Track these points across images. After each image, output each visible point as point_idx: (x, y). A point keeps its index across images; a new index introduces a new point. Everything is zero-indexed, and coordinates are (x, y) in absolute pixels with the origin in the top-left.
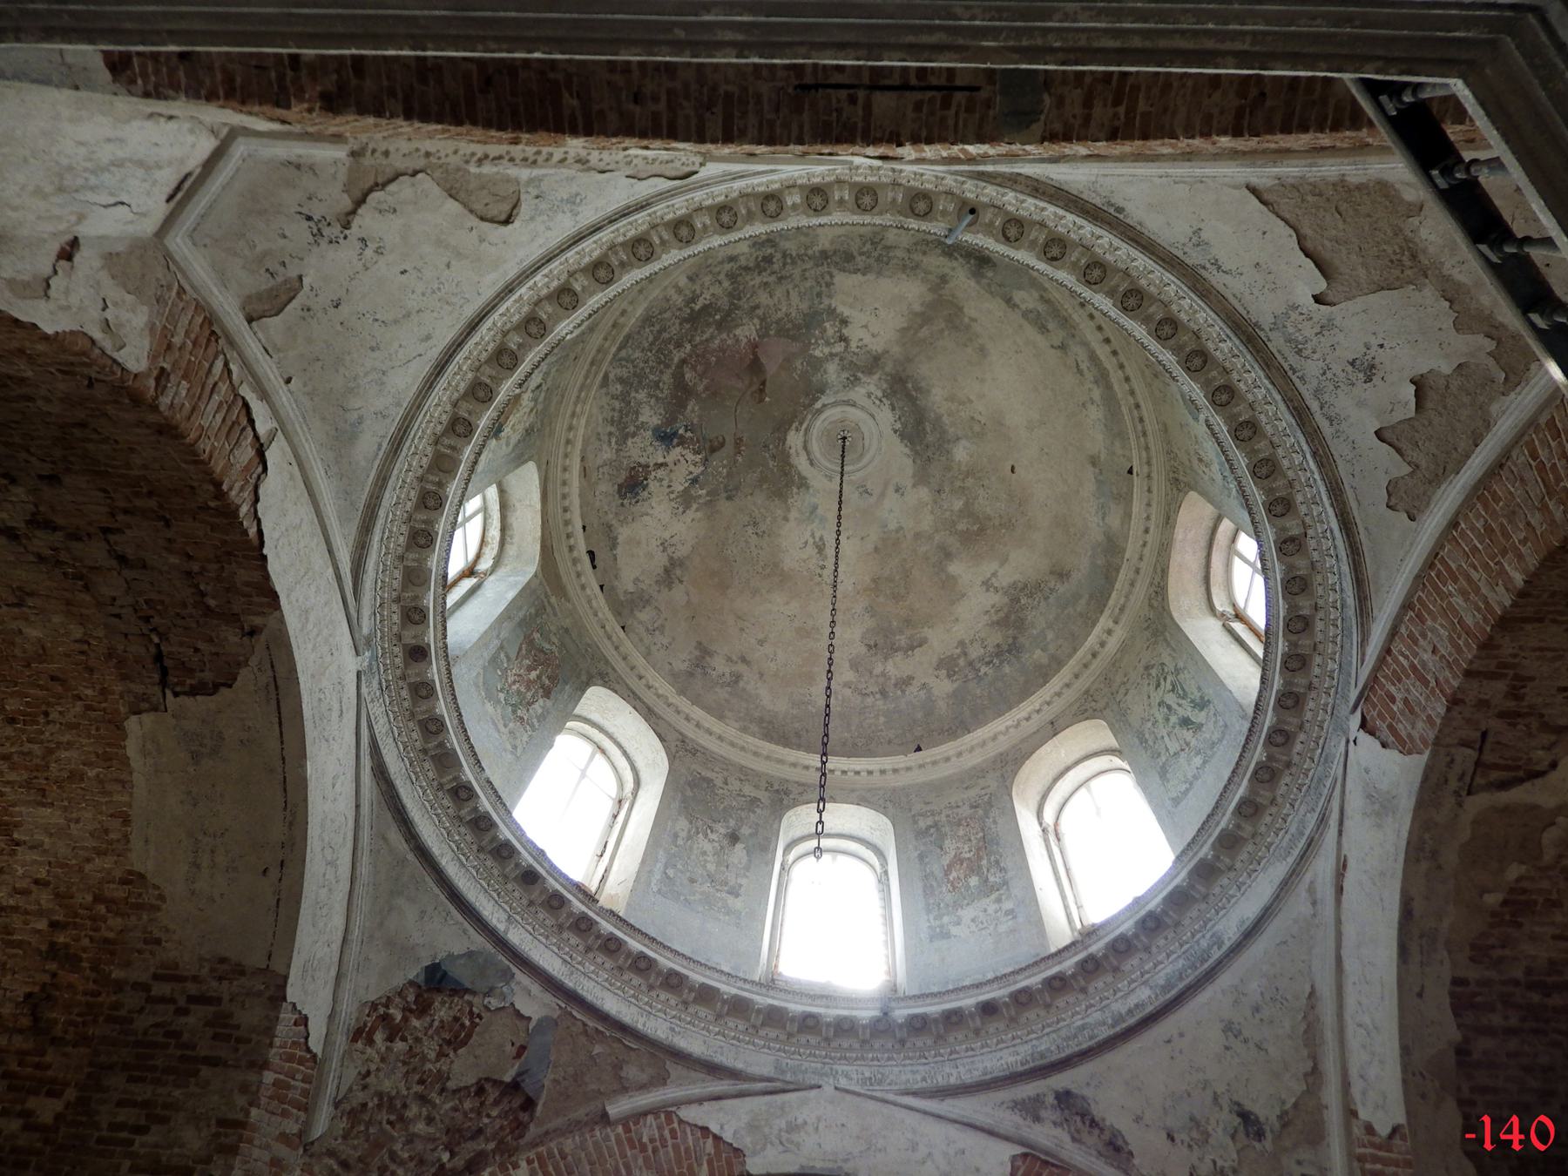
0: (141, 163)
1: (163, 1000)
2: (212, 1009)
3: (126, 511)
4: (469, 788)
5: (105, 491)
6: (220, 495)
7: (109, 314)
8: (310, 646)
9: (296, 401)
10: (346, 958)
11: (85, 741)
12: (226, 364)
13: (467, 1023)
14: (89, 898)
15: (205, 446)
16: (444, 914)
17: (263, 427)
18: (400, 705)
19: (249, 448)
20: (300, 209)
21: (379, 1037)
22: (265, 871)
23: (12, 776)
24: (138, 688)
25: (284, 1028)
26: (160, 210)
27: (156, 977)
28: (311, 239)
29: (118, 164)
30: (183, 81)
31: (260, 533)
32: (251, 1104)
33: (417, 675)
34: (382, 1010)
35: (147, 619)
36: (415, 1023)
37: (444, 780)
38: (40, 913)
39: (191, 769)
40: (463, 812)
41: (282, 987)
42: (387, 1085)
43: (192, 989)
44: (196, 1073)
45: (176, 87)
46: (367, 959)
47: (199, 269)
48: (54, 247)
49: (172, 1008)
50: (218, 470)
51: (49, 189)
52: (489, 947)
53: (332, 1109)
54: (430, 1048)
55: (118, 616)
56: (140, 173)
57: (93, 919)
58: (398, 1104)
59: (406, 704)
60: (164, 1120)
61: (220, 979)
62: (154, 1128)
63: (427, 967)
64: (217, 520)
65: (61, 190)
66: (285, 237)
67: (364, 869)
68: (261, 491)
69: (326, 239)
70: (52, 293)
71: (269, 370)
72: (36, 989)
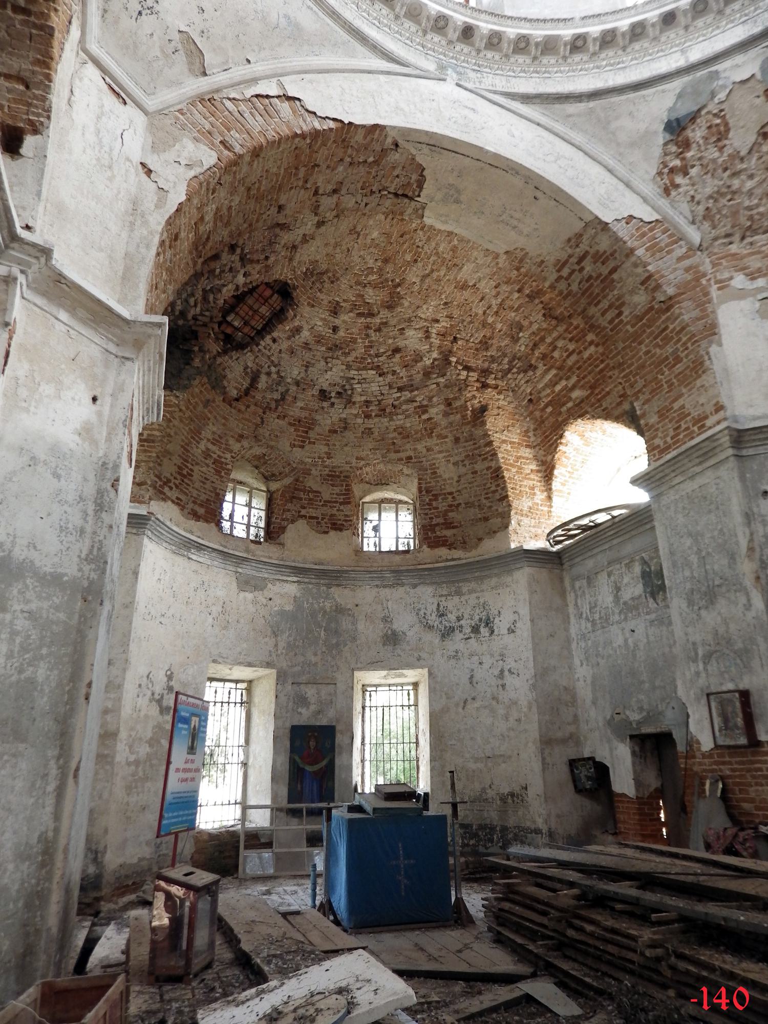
0: (99, 118)
1: (571, 274)
2: (589, 257)
3: (306, 182)
4: (578, 37)
5: (291, 188)
6: (303, 136)
7: (183, 163)
8: (419, 115)
9: (263, 60)
10: (619, 175)
11: (438, 238)
12: (229, 99)
13: (718, 121)
14: (515, 272)
15: (271, 135)
16: (642, 100)
17: (273, 91)
18: (495, 62)
19: (283, 105)
20: (134, 18)
21: (679, 180)
22: (535, 198)
23: (442, 273)
24: (409, 211)
25: (623, 231)
26: (130, 110)
27: (559, 271)
28: (154, 16)
29: (98, 132)
30: (40, 92)
31: (334, 120)
32: (645, 267)
33: (481, 40)
34: (666, 170)
35: (372, 192)
36: (689, 155)
37: (562, 53)
38: (511, 293)
39: (463, 206)
40: (591, 49)
41: (600, 222)
42: (708, 190)
43: (574, 260)
44: (613, 281)
45: (44, 99)
46: (631, 164)
47: (169, 96)
48: (144, 177)
49: (576, 273)
50: (288, 132)
51: (109, 173)
52: (686, 79)
53: (693, 227)
54: (712, 153)
55: (366, 204)
56: (104, 119)
57: (525, 276)
58: (724, 190)
59: (497, 57)
60: (623, 304)
61: (577, 246)
62: (623, 309)
63: (665, 129)
64: (319, 142)
65: (110, 167)
66: (152, 35)
67: (578, 138)
68: (310, 109)
69: (155, 5)
70: (166, 188)
71: (239, 72)
72: (543, 311)
